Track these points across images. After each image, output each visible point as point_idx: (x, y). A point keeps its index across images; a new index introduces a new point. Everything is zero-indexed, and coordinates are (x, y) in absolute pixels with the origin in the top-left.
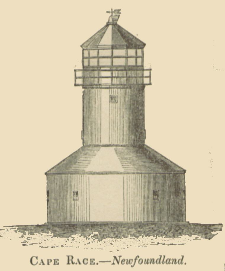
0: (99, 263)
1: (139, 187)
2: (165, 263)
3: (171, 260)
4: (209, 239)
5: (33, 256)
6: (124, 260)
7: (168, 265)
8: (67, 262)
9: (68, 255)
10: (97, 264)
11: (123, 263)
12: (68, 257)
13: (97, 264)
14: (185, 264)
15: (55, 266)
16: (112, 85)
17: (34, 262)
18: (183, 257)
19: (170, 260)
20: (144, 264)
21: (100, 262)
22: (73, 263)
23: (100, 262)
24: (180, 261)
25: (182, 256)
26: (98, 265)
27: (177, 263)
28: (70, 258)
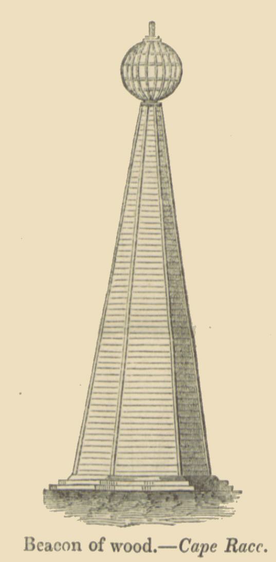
0: (158, 549)
1: (105, 408)
2: (238, 551)
3: (199, 546)
4: (45, 491)
5: (184, 537)
6: (214, 546)
7: (243, 553)
8: (24, 547)
9: (229, 537)
10: (155, 551)
11: (213, 549)
12: (27, 538)
13: (155, 551)
14: (266, 551)
15: (26, 552)
16: (123, 216)
17: (184, 548)
18: (150, 539)
19: (198, 545)
20: (191, 551)
21: (160, 547)
22: (235, 550)
23: (160, 547)
24: (205, 549)
25: (227, 539)
26: (266, 553)
27: (247, 551)
28: (233, 542)
